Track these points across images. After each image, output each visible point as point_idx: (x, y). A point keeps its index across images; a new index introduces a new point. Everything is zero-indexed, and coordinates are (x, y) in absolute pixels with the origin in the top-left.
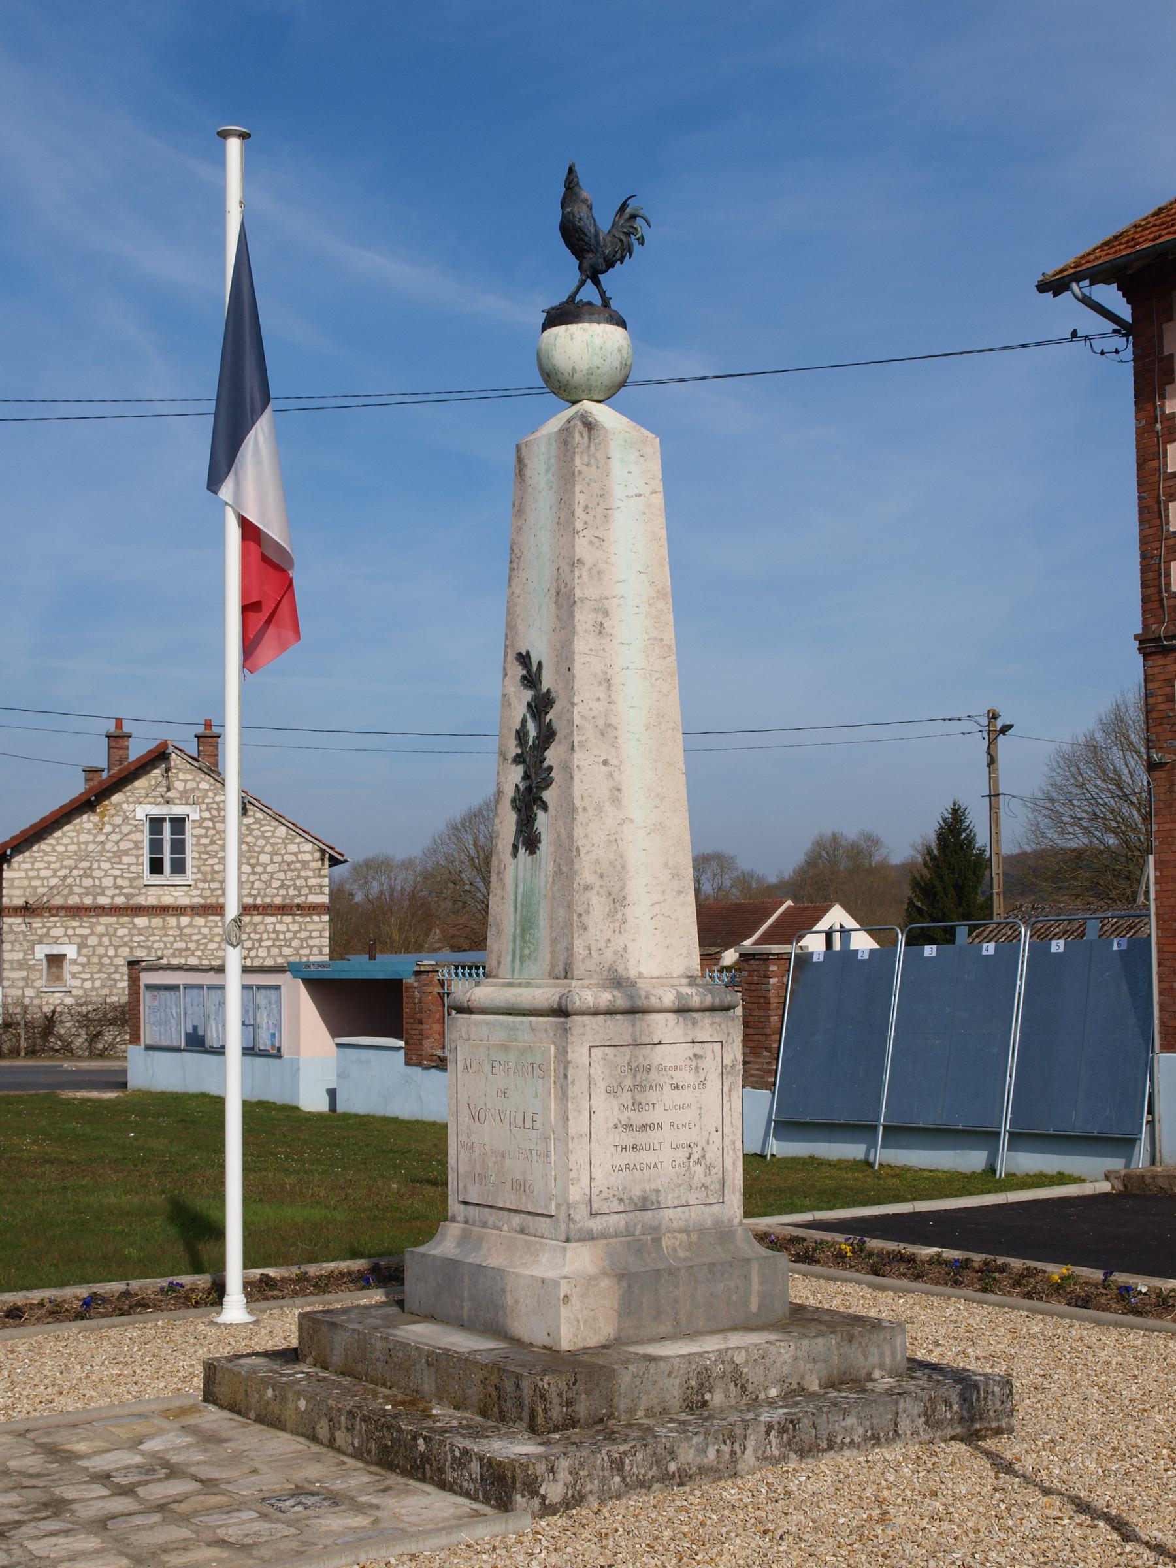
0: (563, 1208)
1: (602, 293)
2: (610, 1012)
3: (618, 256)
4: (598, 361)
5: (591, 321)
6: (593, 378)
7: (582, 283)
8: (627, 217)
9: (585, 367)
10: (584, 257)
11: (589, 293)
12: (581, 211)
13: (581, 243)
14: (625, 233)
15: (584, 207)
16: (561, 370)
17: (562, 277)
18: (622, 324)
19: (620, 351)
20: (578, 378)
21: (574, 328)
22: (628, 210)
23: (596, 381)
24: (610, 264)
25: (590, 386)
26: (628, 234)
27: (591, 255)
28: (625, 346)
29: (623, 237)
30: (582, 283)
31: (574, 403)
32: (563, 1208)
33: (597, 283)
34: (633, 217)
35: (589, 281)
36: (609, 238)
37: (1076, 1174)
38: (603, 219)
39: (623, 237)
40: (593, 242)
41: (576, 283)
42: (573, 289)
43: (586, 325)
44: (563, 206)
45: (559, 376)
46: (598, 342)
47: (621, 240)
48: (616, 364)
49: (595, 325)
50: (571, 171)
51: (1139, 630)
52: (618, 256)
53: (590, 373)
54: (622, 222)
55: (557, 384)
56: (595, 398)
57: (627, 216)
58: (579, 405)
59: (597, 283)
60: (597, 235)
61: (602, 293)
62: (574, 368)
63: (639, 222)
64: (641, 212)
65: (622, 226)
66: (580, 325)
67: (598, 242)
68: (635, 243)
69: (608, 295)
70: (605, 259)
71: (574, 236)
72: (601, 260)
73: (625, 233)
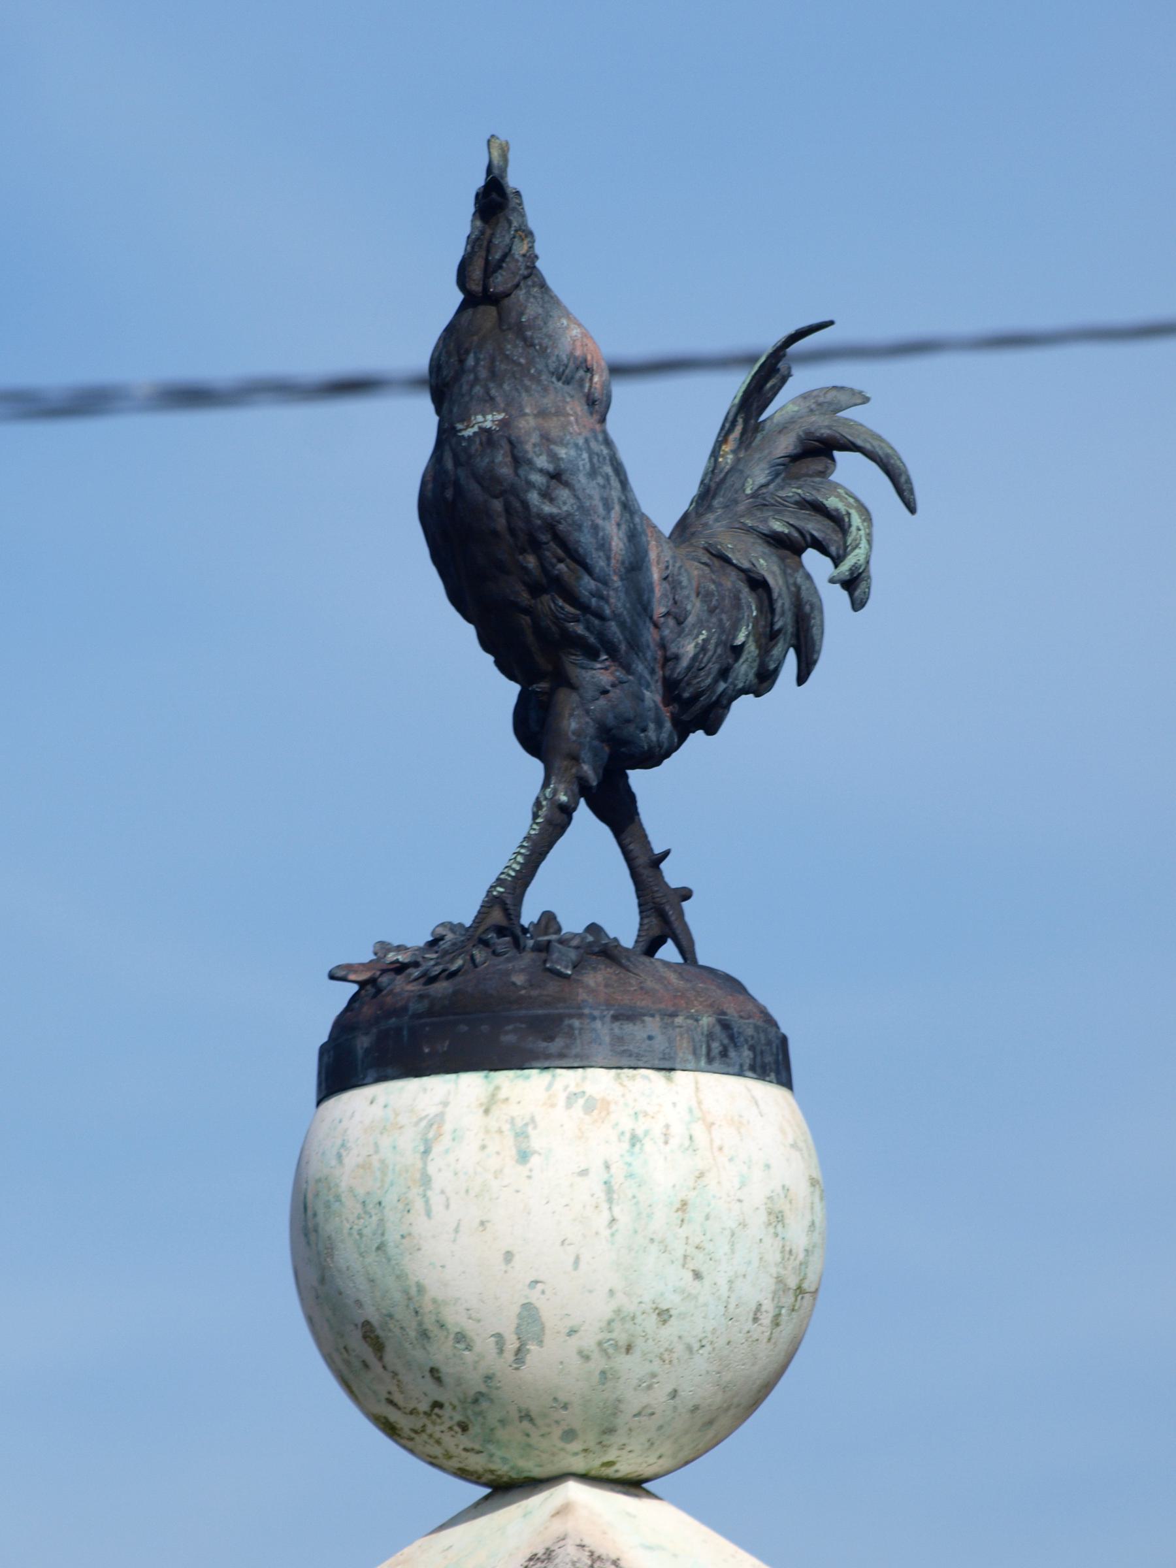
1: (644, 866)
3: (744, 669)
4: (662, 1281)
5: (626, 1058)
6: (631, 1367)
7: (552, 825)
9: (593, 1313)
11: (585, 885)
12: (542, 425)
14: (777, 541)
15: (576, 407)
16: (455, 1318)
17: (421, 772)
19: (777, 1218)
20: (553, 1365)
21: (527, 1091)
23: (648, 1383)
25: (615, 1408)
26: (788, 547)
27: (600, 674)
28: (802, 1190)
29: (767, 565)
30: (552, 825)
31: (505, 1488)
33: (619, 813)
34: (819, 449)
35: (583, 814)
36: (693, 573)
39: (767, 565)
40: (617, 601)
41: (520, 825)
43: (598, 1081)
45: (441, 1352)
46: (665, 1174)
47: (758, 584)
48: (757, 1290)
50: (494, 200)
51: (697, 738)
52: (744, 669)
53: (619, 1343)
54: (757, 476)
55: (421, 1392)
56: (626, 1467)
57: (785, 445)
58: (537, 1507)
59: (619, 813)
61: (644, 866)
62: (529, 1315)
63: (851, 473)
64: (860, 418)
65: (761, 502)
66: (567, 1079)
67: (643, 606)
68: (834, 600)
69: (673, 874)
70: (671, 689)
71: (502, 552)
72: (653, 697)
73: (777, 541)
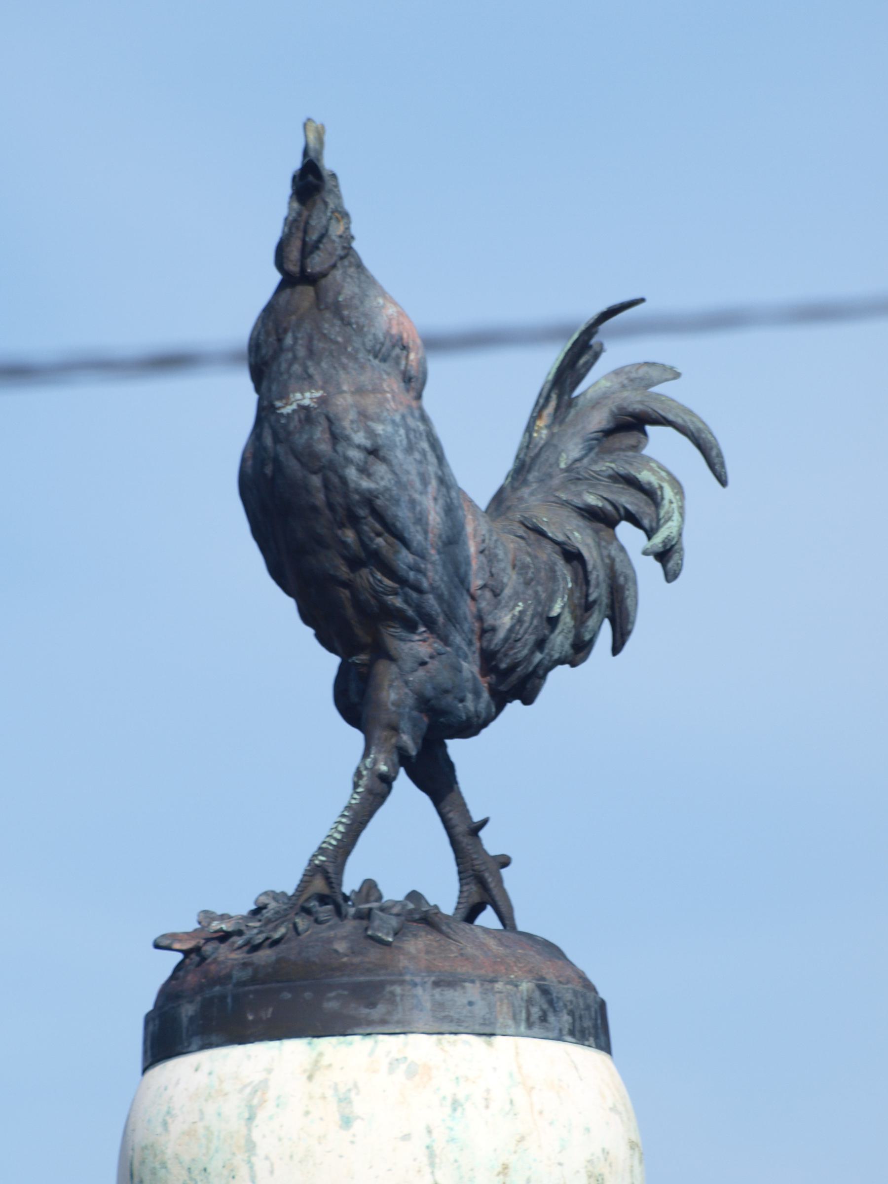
1: (464, 835)
3: (560, 641)
5: (448, 1024)
8: (605, 448)
10: (381, 652)
11: (407, 853)
12: (354, 400)
14: (591, 514)
15: (392, 384)
18: (590, 1025)
24: (515, 682)
26: (602, 519)
27: (418, 645)
28: (621, 1152)
29: (581, 537)
33: (437, 780)
34: (632, 424)
35: (403, 783)
36: (509, 546)
37: (276, 205)
38: (476, 428)
39: (581, 537)
40: (434, 574)
41: (342, 794)
43: (418, 1047)
47: (573, 556)
49: (467, 1046)
52: (560, 641)
54: (572, 450)
59: (437, 780)
61: (464, 835)
63: (663, 446)
66: (387, 1046)
67: (459, 576)
68: (647, 571)
69: (492, 842)
70: (488, 659)
72: (470, 668)
73: (591, 514)
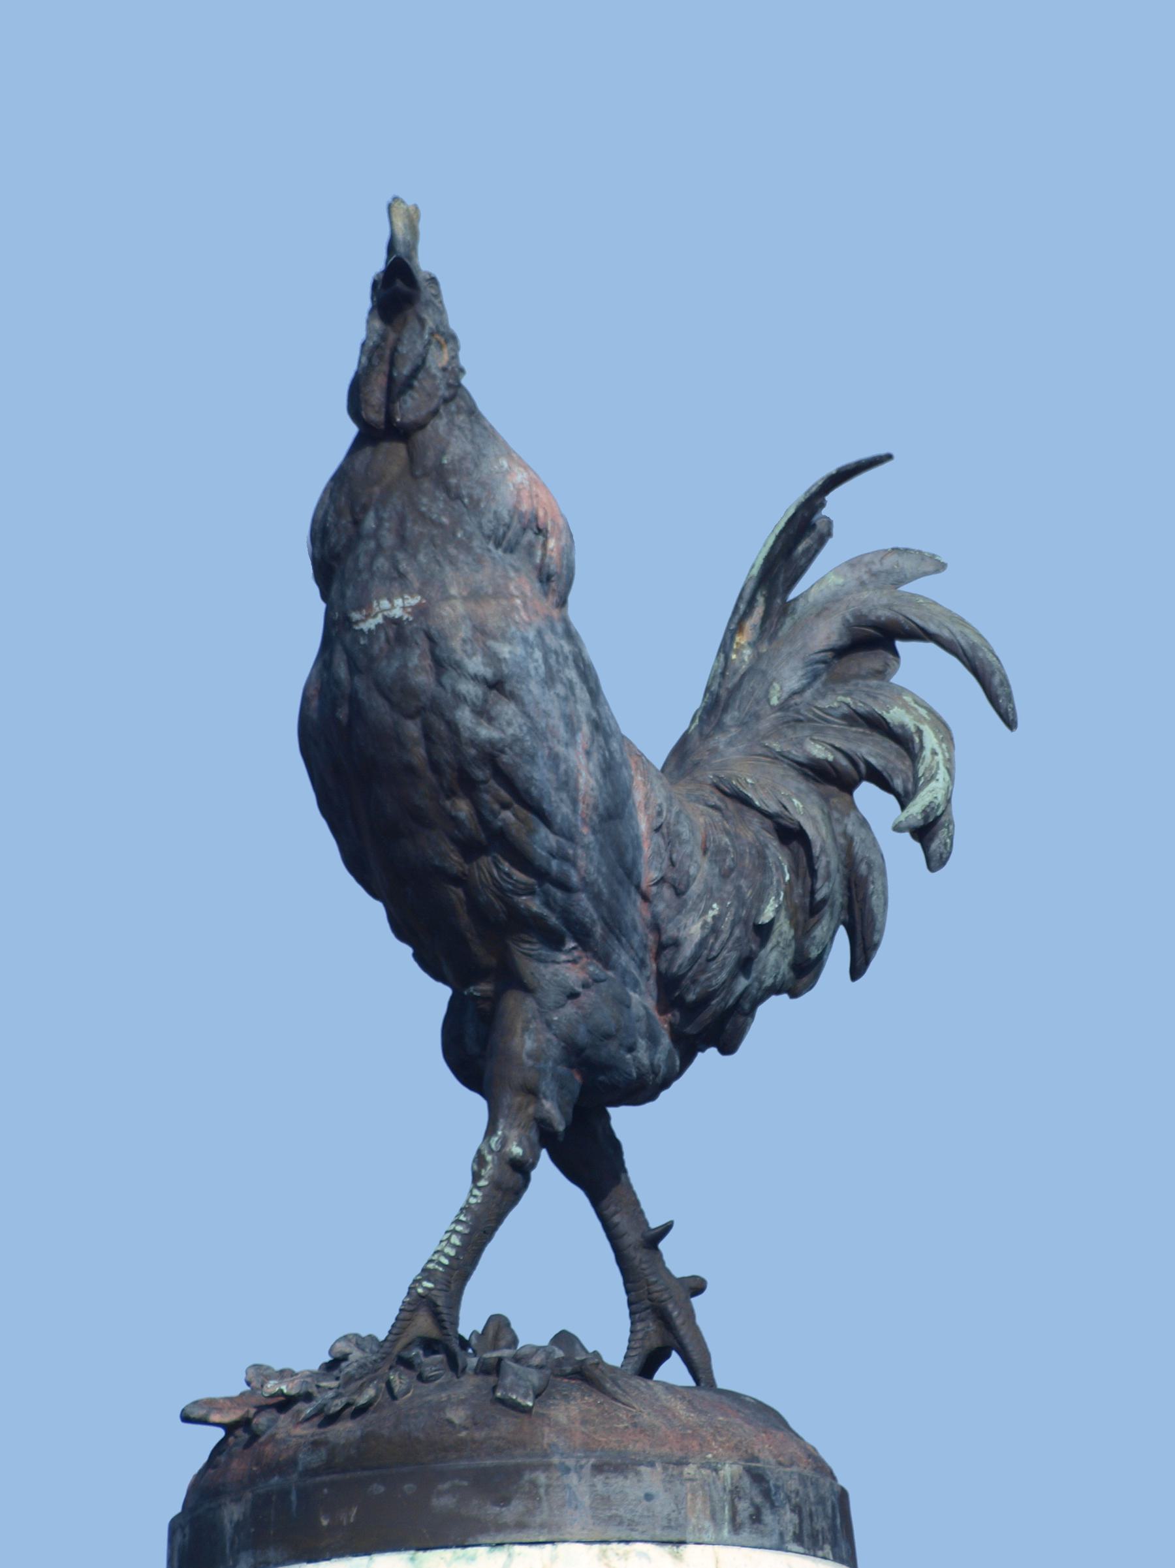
0: (516, 518)
1: (635, 1247)
2: (569, 961)
3: (774, 959)
7: (503, 1188)
8: (838, 668)
11: (550, 1276)
12: (471, 610)
13: (492, 869)
16: (498, 497)
22: (821, 575)
24: (715, 1024)
26: (834, 779)
27: (567, 969)
29: (803, 806)
30: (503, 1188)
32: (516, 518)
33: (596, 1168)
34: (875, 638)
35: (546, 1171)
36: (698, 820)
38: (645, 644)
39: (803, 806)
40: (588, 864)
42: (429, 1235)
44: (336, 556)
47: (791, 835)
50: (399, 291)
52: (774, 959)
54: (788, 678)
57: (826, 633)
59: (596, 1168)
60: (613, 813)
61: (635, 1247)
63: (920, 669)
65: (792, 715)
68: (901, 856)
70: (669, 989)
71: (421, 798)
72: (643, 1000)
